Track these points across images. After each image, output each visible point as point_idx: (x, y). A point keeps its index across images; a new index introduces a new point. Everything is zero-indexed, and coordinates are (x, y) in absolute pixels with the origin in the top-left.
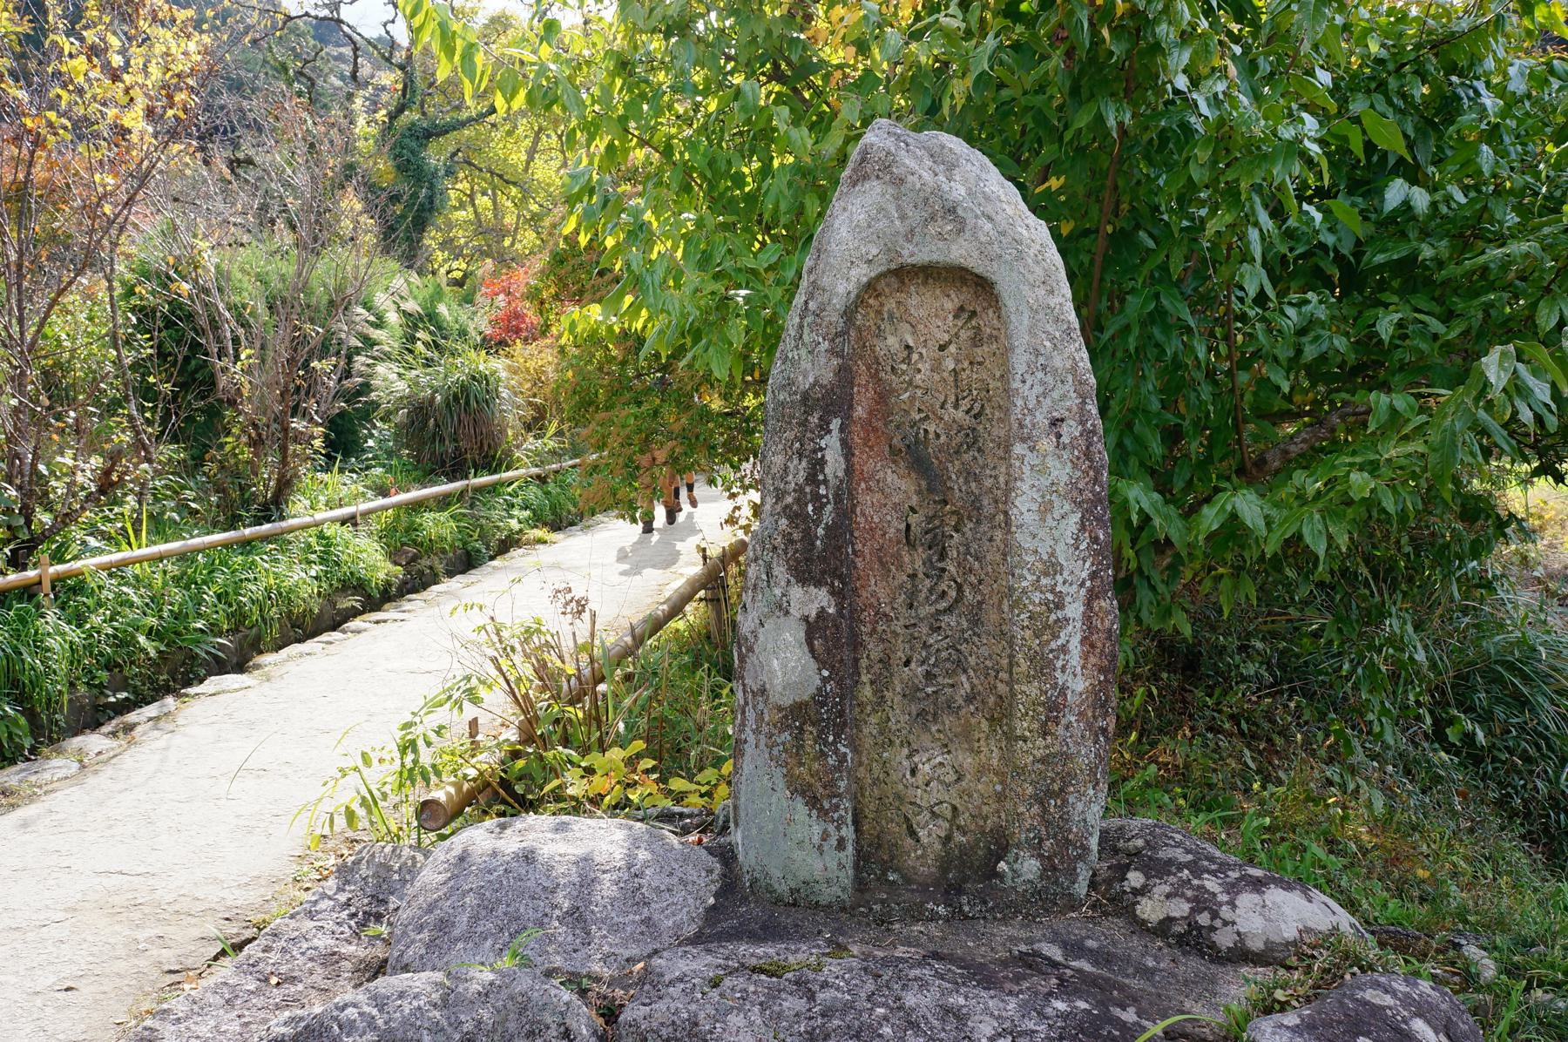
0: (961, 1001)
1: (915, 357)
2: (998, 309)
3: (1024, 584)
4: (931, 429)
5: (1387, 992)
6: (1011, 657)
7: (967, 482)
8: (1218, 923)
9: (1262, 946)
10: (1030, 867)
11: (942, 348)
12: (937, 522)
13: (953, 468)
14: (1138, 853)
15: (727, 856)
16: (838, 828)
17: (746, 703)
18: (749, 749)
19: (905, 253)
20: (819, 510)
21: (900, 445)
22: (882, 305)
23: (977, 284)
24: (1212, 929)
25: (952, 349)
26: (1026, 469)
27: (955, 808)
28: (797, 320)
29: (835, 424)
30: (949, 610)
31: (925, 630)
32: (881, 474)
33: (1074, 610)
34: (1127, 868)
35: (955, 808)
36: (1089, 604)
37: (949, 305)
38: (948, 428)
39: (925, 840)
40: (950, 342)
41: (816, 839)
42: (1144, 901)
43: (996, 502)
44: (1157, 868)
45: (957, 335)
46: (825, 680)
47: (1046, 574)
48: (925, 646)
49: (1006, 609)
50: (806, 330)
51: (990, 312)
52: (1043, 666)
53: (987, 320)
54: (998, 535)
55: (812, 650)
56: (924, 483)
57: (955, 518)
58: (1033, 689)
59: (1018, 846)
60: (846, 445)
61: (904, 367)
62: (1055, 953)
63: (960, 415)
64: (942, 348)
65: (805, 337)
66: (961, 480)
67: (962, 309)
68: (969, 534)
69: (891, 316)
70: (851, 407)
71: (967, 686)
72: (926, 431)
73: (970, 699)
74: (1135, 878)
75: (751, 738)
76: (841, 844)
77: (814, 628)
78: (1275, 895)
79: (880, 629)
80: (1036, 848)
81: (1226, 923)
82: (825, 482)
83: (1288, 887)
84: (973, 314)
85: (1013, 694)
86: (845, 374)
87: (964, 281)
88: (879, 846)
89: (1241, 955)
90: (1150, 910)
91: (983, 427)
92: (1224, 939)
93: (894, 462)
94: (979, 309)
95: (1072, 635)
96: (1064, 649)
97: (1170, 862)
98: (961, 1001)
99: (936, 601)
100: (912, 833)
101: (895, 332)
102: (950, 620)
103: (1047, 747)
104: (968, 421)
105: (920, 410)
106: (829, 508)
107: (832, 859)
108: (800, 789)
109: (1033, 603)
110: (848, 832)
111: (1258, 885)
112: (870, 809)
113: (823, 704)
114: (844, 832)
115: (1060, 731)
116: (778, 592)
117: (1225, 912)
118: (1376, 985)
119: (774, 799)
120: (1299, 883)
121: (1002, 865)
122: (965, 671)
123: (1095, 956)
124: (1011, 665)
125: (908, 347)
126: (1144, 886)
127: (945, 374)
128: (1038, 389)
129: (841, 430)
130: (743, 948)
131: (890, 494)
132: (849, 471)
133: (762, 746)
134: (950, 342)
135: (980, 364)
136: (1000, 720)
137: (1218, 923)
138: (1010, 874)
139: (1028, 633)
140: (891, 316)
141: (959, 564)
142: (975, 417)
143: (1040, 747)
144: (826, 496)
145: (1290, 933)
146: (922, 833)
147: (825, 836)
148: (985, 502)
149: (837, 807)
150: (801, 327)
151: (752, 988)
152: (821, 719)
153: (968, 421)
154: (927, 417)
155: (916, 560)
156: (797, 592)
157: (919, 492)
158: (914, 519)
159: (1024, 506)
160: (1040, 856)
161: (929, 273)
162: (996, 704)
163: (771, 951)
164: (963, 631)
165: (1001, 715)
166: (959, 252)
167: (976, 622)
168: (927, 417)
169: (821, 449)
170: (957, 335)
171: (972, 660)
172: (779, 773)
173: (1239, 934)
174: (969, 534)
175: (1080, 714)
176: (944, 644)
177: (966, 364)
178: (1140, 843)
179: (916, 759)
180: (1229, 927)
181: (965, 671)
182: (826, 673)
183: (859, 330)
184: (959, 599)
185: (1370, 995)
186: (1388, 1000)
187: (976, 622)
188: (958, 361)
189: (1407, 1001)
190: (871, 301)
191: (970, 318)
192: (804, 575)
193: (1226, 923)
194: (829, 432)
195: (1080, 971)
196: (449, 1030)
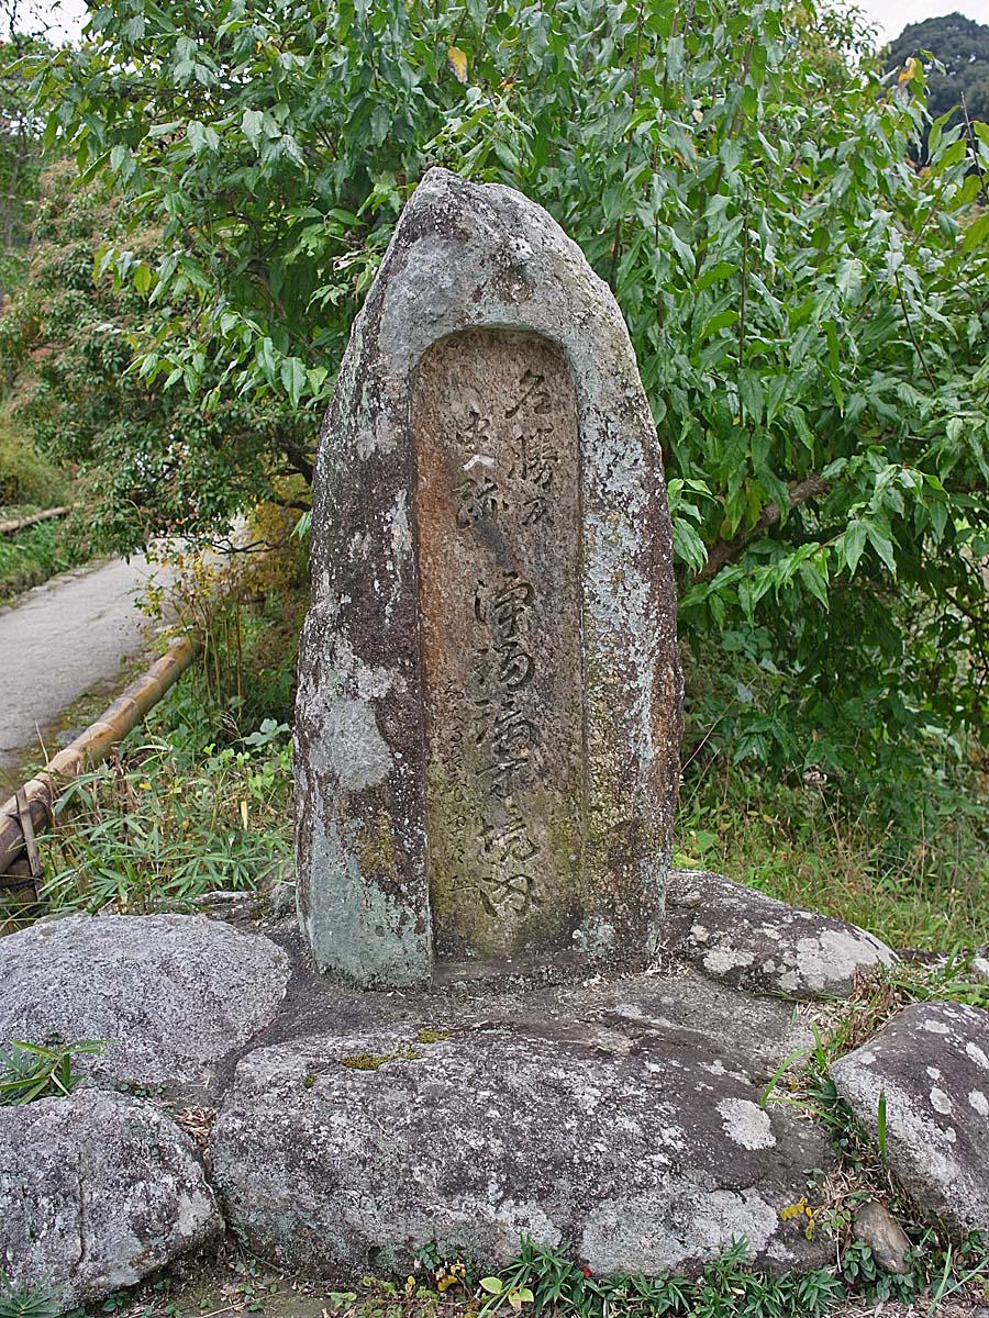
0: (562, 1075)
1: (481, 424)
2: (566, 375)
3: (599, 656)
4: (499, 500)
5: (942, 1021)
6: (584, 729)
7: (537, 554)
8: (782, 969)
9: (822, 986)
10: (605, 931)
11: (509, 414)
12: (507, 596)
13: (523, 539)
14: (696, 905)
15: (294, 943)
16: (417, 911)
17: (311, 788)
18: (318, 837)
19: (473, 314)
20: (386, 587)
21: (470, 517)
22: (446, 369)
23: (544, 348)
24: (778, 975)
25: (519, 415)
26: (599, 541)
27: (530, 881)
28: (354, 384)
29: (400, 497)
30: (520, 685)
31: (497, 705)
32: (449, 547)
33: (645, 679)
34: (691, 920)
35: (530, 881)
36: (657, 673)
37: (515, 370)
38: (516, 498)
39: (502, 914)
40: (517, 407)
41: (395, 924)
42: (712, 954)
43: (566, 573)
44: (714, 919)
45: (523, 401)
46: (397, 764)
47: (619, 646)
48: (498, 722)
49: (578, 681)
50: (365, 395)
51: (558, 376)
52: (617, 733)
53: (555, 387)
54: (570, 608)
55: (383, 733)
56: (492, 556)
57: (525, 591)
58: (606, 760)
59: (591, 913)
60: (412, 518)
61: (470, 435)
62: (634, 1013)
63: (528, 484)
64: (509, 414)
65: (364, 403)
66: (531, 552)
67: (528, 373)
68: (540, 607)
69: (455, 382)
70: (416, 479)
71: (540, 759)
72: (493, 501)
73: (542, 773)
74: (699, 932)
75: (320, 825)
76: (420, 929)
77: (383, 707)
78: (829, 937)
79: (450, 707)
80: (609, 912)
81: (789, 969)
82: (392, 557)
83: (839, 929)
84: (541, 378)
85: (587, 766)
86: (409, 442)
87: (530, 344)
88: (456, 923)
89: (806, 996)
90: (720, 960)
91: (560, 503)
92: (788, 983)
93: (461, 534)
94: (546, 374)
95: (644, 705)
96: (636, 719)
97: (731, 910)
98: (562, 1075)
99: (508, 676)
100: (490, 909)
101: (460, 398)
102: (523, 694)
103: (620, 815)
104: (536, 490)
105: (487, 480)
106: (397, 584)
107: (411, 941)
108: (375, 875)
109: (607, 675)
110: (426, 914)
111: (811, 929)
112: (446, 889)
113: (395, 788)
114: (423, 913)
115: (631, 798)
116: (344, 674)
117: (787, 957)
118: (932, 1015)
119: (349, 887)
120: (843, 922)
121: (577, 934)
122: (538, 745)
123: (678, 1013)
124: (584, 736)
125: (473, 413)
126: (710, 939)
127: (513, 443)
128: (610, 458)
129: (407, 502)
130: (331, 1042)
131: (459, 570)
132: (416, 543)
133: (333, 832)
134: (517, 407)
135: (549, 431)
136: (573, 791)
137: (782, 969)
138: (585, 940)
139: (602, 705)
140: (455, 382)
141: (530, 638)
142: (544, 486)
143: (614, 815)
144: (393, 572)
145: (846, 971)
146: (498, 907)
147: (404, 920)
148: (556, 574)
149: (415, 891)
150: (359, 389)
151: (349, 1083)
152: (395, 802)
153: (536, 490)
154: (495, 487)
155: (486, 635)
156: (364, 674)
157: (489, 565)
158: (483, 593)
159: (598, 577)
160: (614, 920)
161: (495, 337)
162: (569, 776)
163: (362, 1043)
164: (536, 705)
165: (574, 786)
166: (531, 314)
167: (547, 695)
168: (495, 487)
169: (386, 522)
170: (523, 401)
171: (545, 734)
172: (352, 861)
173: (801, 977)
174: (540, 607)
175: (650, 779)
176: (516, 719)
177: (534, 432)
178: (697, 895)
179: (491, 834)
180: (793, 972)
181: (538, 745)
182: (399, 756)
183: (421, 394)
184: (529, 675)
185: (931, 1026)
186: (944, 1029)
187: (547, 695)
188: (525, 429)
189: (958, 1026)
190: (434, 365)
191: (538, 383)
192: (372, 655)
193: (789, 969)
194: (395, 503)
195: (664, 1029)
196: (31, 1169)
